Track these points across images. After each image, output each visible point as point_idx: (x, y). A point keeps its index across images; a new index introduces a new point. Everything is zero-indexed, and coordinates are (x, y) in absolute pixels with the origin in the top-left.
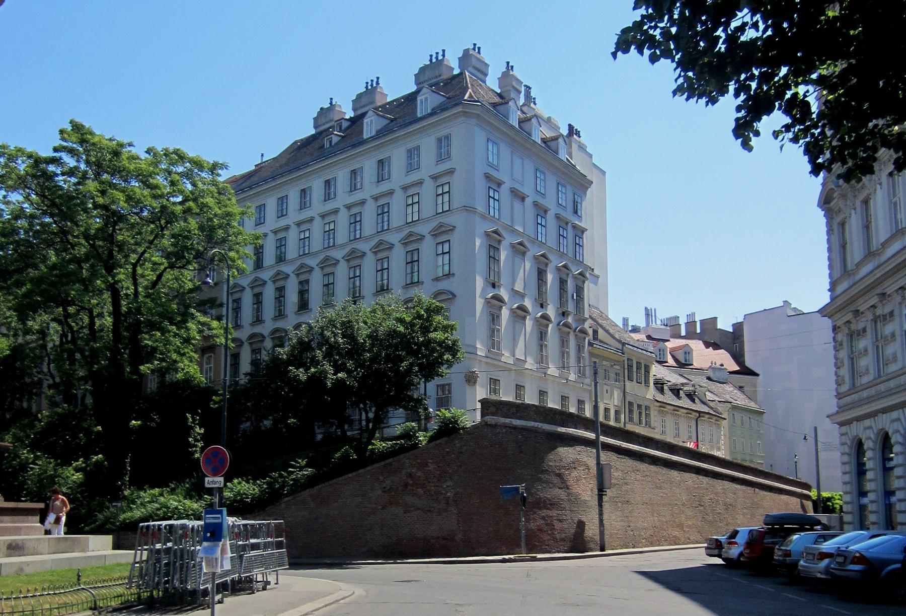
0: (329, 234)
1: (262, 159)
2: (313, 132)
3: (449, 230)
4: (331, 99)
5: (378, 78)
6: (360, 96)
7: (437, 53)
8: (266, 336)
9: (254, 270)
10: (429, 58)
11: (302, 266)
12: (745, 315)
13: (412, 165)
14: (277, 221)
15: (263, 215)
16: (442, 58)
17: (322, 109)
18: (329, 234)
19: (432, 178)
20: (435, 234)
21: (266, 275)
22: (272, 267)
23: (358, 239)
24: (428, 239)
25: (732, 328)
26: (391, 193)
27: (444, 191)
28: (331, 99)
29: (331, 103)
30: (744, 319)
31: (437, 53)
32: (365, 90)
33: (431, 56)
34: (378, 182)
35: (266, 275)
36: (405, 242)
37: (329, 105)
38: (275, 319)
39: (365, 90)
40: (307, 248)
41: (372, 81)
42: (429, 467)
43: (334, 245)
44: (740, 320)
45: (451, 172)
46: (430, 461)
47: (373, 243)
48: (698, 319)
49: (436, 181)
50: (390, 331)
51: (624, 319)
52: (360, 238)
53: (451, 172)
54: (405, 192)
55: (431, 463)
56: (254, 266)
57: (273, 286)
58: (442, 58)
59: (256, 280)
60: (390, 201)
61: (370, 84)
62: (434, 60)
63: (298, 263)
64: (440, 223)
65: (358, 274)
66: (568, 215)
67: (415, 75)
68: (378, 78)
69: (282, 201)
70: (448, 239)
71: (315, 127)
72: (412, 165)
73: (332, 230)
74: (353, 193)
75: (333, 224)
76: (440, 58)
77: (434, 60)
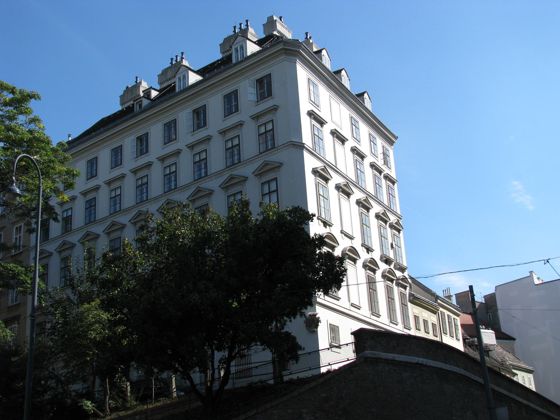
0: (115, 200)
2: (119, 108)
3: (276, 167)
4: (137, 78)
6: (165, 72)
9: (62, 234)
11: (113, 224)
12: (496, 287)
13: (92, 173)
14: (163, 149)
15: (95, 168)
17: (127, 87)
18: (115, 200)
19: (189, 147)
20: (259, 174)
21: (51, 247)
22: (81, 228)
23: (203, 177)
24: (79, 247)
25: (483, 299)
26: (208, 139)
27: (201, 158)
28: (137, 78)
29: (136, 82)
30: (495, 290)
32: (170, 65)
33: (235, 27)
34: (257, 102)
35: (74, 238)
36: (225, 187)
43: (147, 200)
44: (492, 291)
46: (304, 410)
48: (453, 293)
49: (85, 196)
52: (120, 210)
54: (224, 136)
56: (62, 229)
59: (65, 244)
60: (148, 173)
61: (175, 59)
62: (174, 62)
63: (108, 222)
64: (168, 199)
66: (380, 163)
69: (117, 153)
70: (275, 177)
71: (122, 104)
72: (92, 173)
73: (118, 195)
74: (139, 158)
75: (204, 153)
76: (243, 27)
77: (174, 62)
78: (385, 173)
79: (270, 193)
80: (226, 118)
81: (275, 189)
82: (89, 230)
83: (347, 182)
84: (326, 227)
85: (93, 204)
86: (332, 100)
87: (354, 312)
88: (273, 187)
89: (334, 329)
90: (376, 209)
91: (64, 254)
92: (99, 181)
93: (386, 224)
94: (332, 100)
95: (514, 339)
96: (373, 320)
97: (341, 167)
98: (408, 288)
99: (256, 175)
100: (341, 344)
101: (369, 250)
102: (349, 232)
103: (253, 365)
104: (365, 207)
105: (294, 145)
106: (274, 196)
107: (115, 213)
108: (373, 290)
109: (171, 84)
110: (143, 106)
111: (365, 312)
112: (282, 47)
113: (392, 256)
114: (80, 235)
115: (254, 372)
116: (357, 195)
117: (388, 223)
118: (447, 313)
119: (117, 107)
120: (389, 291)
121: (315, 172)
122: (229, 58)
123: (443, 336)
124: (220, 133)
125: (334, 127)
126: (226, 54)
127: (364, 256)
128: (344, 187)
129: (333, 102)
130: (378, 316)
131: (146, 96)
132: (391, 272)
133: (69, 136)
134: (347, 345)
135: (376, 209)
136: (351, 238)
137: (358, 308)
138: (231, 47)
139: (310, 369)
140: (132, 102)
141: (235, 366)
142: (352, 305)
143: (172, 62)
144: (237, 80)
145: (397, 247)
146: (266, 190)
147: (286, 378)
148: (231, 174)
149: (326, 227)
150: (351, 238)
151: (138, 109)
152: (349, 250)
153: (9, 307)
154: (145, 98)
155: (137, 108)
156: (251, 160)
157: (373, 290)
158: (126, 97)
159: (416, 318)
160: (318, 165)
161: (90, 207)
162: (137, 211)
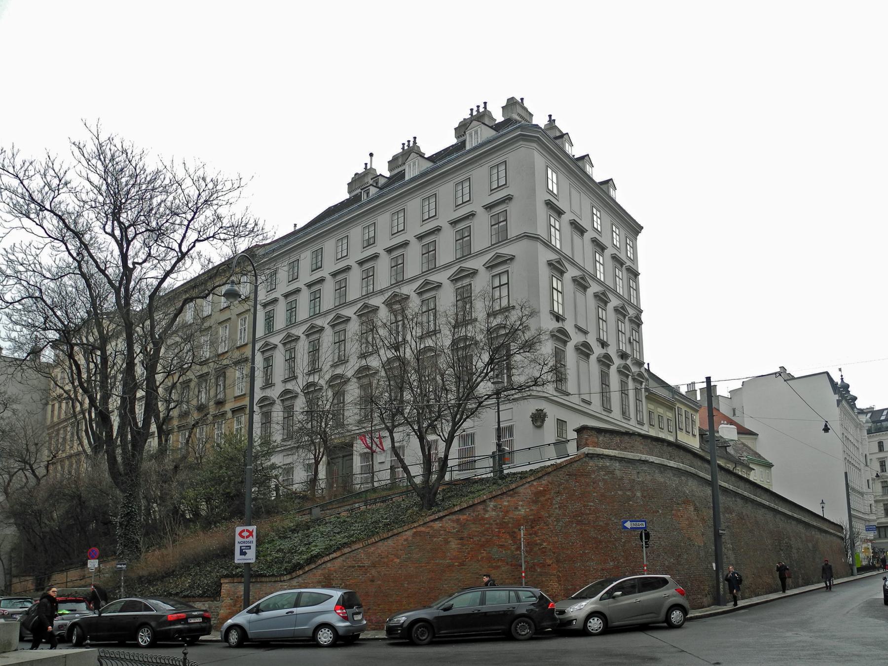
1: (295, 228)
2: (347, 196)
5: (415, 138)
6: (395, 158)
7: (478, 107)
8: (276, 399)
10: (402, 146)
15: (296, 271)
16: (483, 110)
20: (490, 267)
22: (305, 321)
31: (478, 107)
32: (402, 150)
33: (472, 110)
36: (454, 280)
37: (470, 116)
38: (263, 388)
39: (470, 116)
40: (317, 308)
41: (409, 141)
42: (520, 511)
45: (508, 199)
47: (331, 317)
50: (236, 436)
51: (707, 378)
53: (508, 199)
55: (522, 506)
57: (452, 286)
58: (483, 110)
61: (407, 144)
65: (293, 356)
67: (456, 129)
68: (415, 138)
70: (506, 269)
71: (349, 192)
77: (406, 148)
78: (627, 265)
79: (500, 286)
80: (424, 223)
81: (507, 282)
82: (339, 312)
83: (584, 275)
84: (559, 322)
85: (318, 296)
86: (572, 190)
87: (584, 407)
88: (504, 280)
89: (561, 423)
90: (614, 302)
91: (267, 354)
92: (325, 273)
93: (625, 318)
94: (572, 190)
95: (757, 435)
96: (604, 415)
97: (578, 259)
98: (644, 384)
99: (452, 281)
100: (568, 439)
101: (604, 344)
102: (584, 327)
103: (476, 458)
104: (601, 300)
105: (527, 236)
106: (504, 292)
107: (399, 283)
108: (606, 385)
109: (402, 171)
110: (371, 194)
111: (596, 406)
112: (520, 132)
113: (629, 352)
114: (305, 327)
115: (477, 465)
116: (594, 288)
117: (627, 317)
118: (684, 408)
119: (344, 195)
120: (623, 384)
121: (550, 264)
122: (401, 175)
123: (678, 431)
124: (451, 224)
125: (573, 217)
126: (396, 171)
127: (598, 351)
128: (580, 280)
129: (574, 192)
130: (610, 411)
131: (375, 185)
132: (626, 367)
133: (295, 225)
134: (549, 445)
135: (614, 302)
136: (585, 333)
137: (589, 403)
138: (465, 132)
139: (549, 460)
140: (359, 190)
141: (459, 458)
142: (584, 401)
143: (404, 147)
144: (470, 167)
145: (634, 342)
146: (497, 283)
147: (506, 472)
148: (460, 267)
149: (559, 322)
150: (585, 333)
151: (365, 197)
152: (582, 345)
153: (235, 398)
154: (373, 186)
155: (364, 198)
156: (280, 332)
157: (606, 385)
158: (354, 185)
159: (650, 413)
160: (553, 256)
161: (314, 299)
162: (335, 314)
